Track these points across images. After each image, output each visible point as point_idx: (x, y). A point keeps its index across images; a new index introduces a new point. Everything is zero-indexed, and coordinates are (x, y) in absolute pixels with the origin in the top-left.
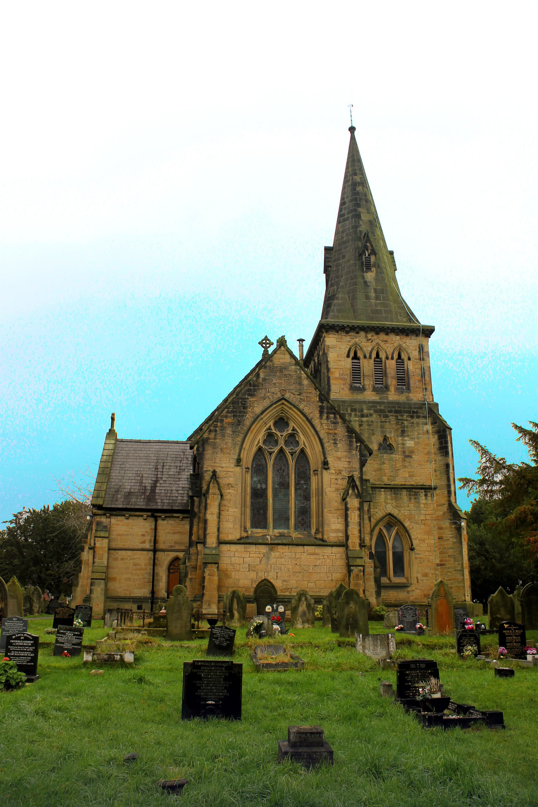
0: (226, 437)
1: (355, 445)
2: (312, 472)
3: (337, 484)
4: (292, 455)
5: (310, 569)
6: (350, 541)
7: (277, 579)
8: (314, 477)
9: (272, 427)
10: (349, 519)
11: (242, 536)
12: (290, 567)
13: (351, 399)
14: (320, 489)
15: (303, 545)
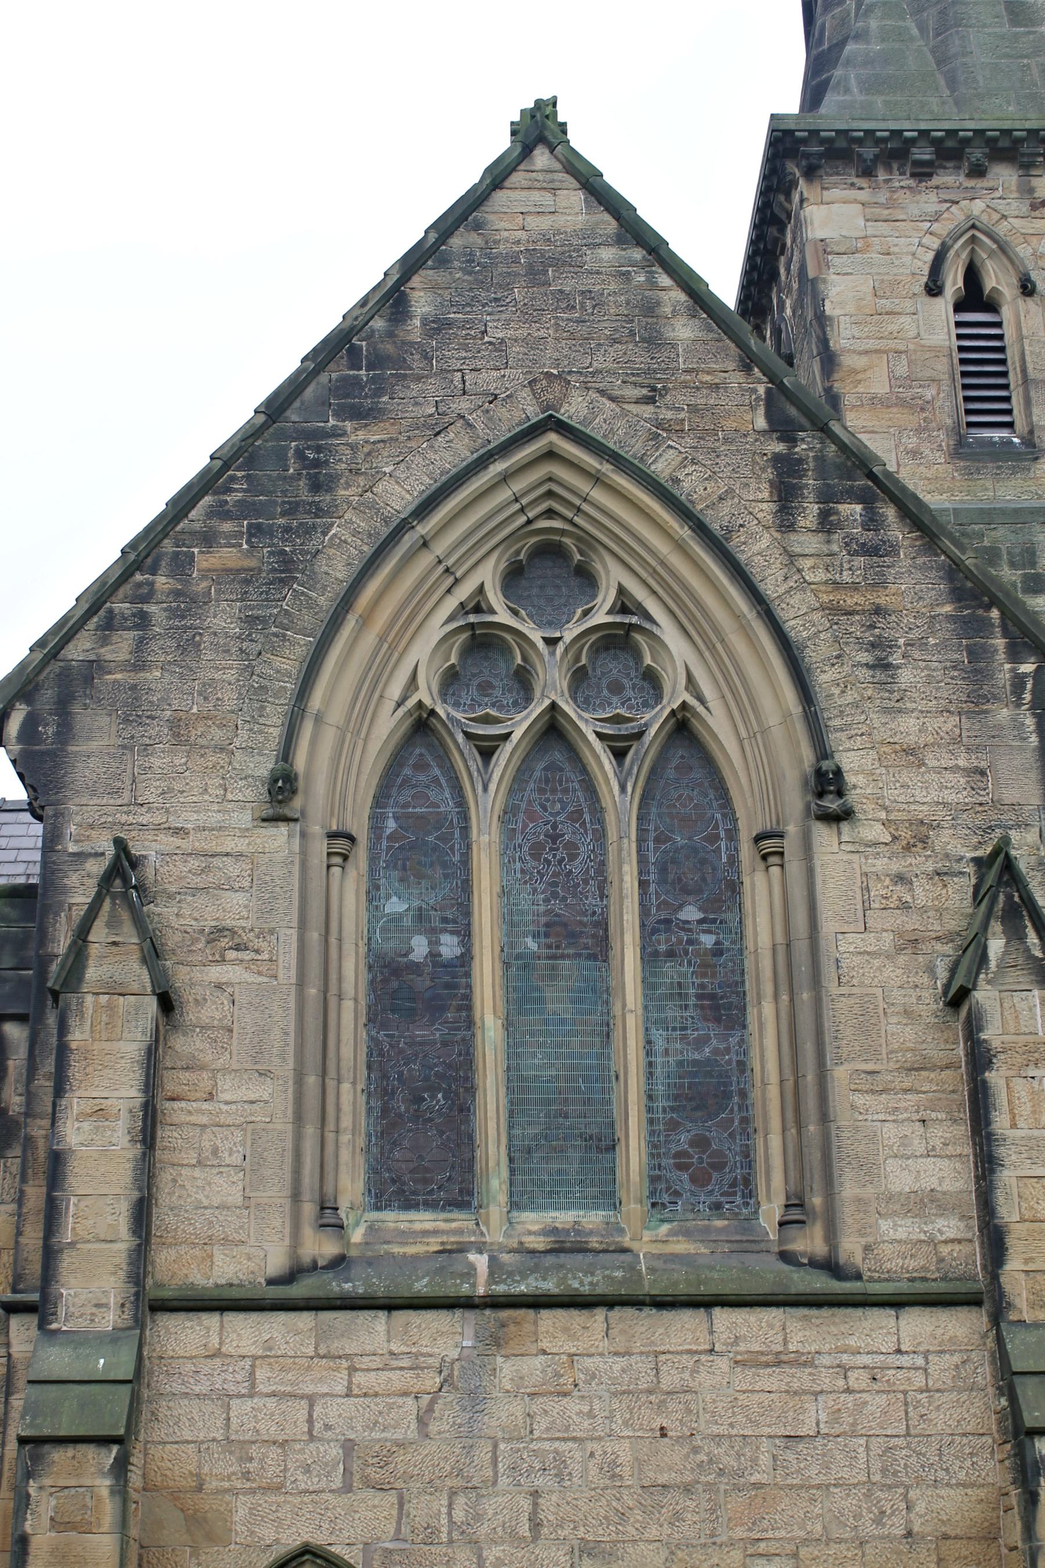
0: (208, 655)
1: (1004, 671)
2: (746, 851)
3: (905, 906)
4: (619, 755)
5: (755, 1461)
6: (1014, 1264)
7: (535, 1538)
8: (760, 877)
9: (495, 598)
10: (1000, 1122)
11: (307, 1260)
12: (624, 1453)
13: (962, 501)
14: (801, 947)
15: (706, 1303)
